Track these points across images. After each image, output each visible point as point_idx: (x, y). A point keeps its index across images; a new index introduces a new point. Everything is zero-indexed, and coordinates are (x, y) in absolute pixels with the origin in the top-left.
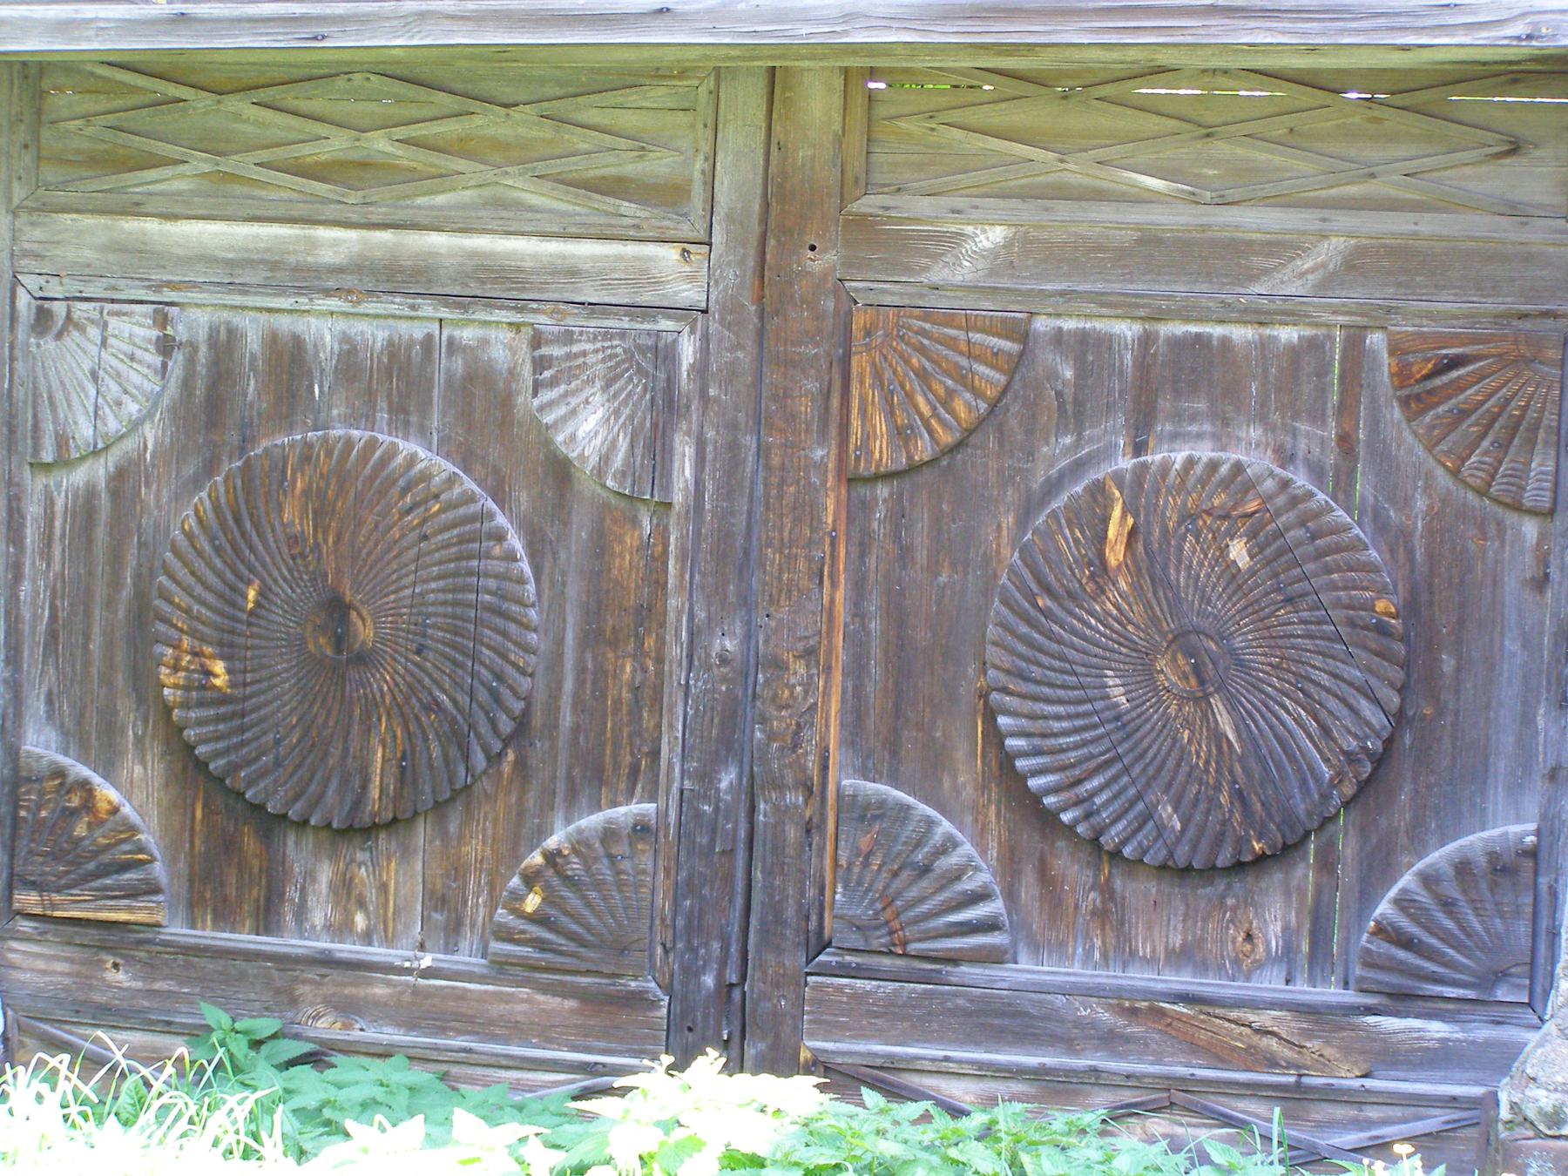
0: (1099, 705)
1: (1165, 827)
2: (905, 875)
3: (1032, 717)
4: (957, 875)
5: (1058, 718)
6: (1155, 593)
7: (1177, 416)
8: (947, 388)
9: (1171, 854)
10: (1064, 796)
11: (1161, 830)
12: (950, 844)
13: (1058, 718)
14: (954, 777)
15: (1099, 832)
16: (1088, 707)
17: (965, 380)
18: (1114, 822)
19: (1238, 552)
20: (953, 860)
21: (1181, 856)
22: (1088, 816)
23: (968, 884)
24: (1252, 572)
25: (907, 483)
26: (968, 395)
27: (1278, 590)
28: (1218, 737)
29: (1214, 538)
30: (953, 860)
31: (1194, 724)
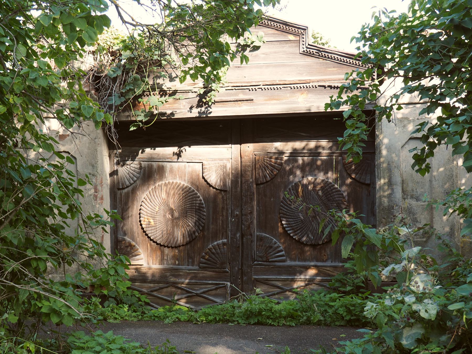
12: (276, 243)
13: (292, 221)
21: (313, 242)
23: (279, 249)
30: (276, 245)
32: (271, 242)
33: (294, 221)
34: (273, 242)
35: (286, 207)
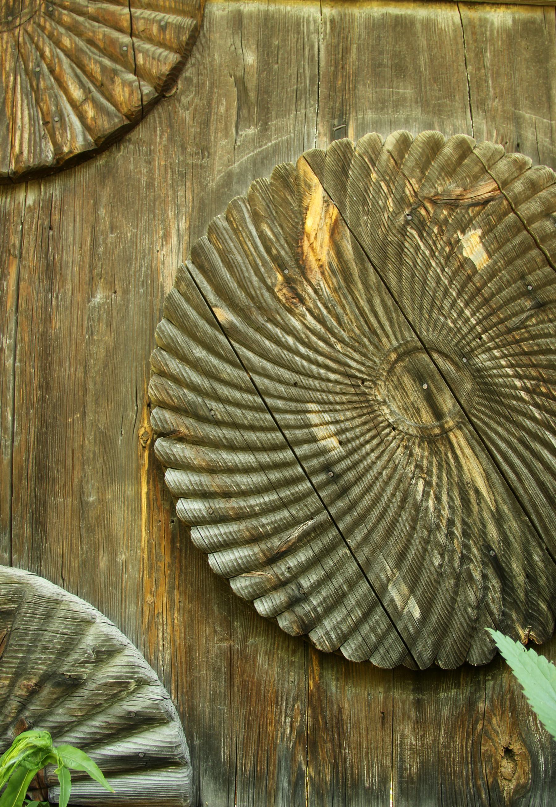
0: (303, 450)
1: (400, 615)
2: (46, 691)
3: (211, 470)
4: (120, 688)
5: (247, 470)
6: (370, 302)
7: (381, 105)
8: (104, 68)
9: (408, 652)
10: (258, 576)
11: (393, 618)
12: (105, 653)
13: (247, 470)
14: (113, 555)
15: (308, 626)
16: (288, 455)
17: (125, 59)
18: (329, 610)
19: (473, 247)
20: (112, 670)
21: (423, 652)
22: (292, 603)
23: (136, 704)
24: (492, 273)
25: (55, 190)
26: (131, 77)
27: (527, 294)
28: (464, 489)
29: (441, 232)
30: (112, 670)
31: (429, 473)
32: (70, 644)
33: (263, 468)
34: (89, 640)
35: (199, 353)
